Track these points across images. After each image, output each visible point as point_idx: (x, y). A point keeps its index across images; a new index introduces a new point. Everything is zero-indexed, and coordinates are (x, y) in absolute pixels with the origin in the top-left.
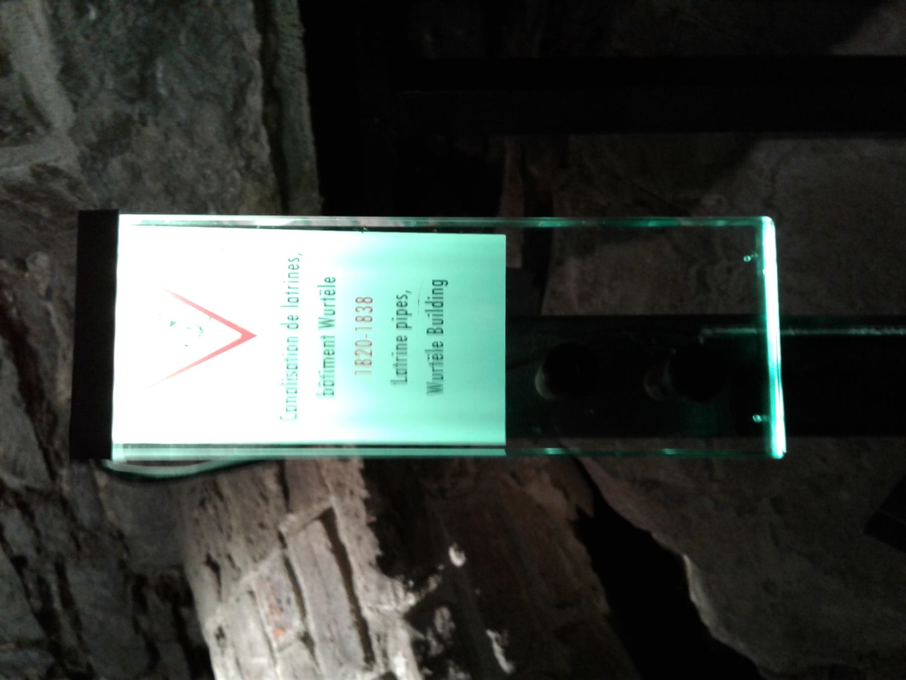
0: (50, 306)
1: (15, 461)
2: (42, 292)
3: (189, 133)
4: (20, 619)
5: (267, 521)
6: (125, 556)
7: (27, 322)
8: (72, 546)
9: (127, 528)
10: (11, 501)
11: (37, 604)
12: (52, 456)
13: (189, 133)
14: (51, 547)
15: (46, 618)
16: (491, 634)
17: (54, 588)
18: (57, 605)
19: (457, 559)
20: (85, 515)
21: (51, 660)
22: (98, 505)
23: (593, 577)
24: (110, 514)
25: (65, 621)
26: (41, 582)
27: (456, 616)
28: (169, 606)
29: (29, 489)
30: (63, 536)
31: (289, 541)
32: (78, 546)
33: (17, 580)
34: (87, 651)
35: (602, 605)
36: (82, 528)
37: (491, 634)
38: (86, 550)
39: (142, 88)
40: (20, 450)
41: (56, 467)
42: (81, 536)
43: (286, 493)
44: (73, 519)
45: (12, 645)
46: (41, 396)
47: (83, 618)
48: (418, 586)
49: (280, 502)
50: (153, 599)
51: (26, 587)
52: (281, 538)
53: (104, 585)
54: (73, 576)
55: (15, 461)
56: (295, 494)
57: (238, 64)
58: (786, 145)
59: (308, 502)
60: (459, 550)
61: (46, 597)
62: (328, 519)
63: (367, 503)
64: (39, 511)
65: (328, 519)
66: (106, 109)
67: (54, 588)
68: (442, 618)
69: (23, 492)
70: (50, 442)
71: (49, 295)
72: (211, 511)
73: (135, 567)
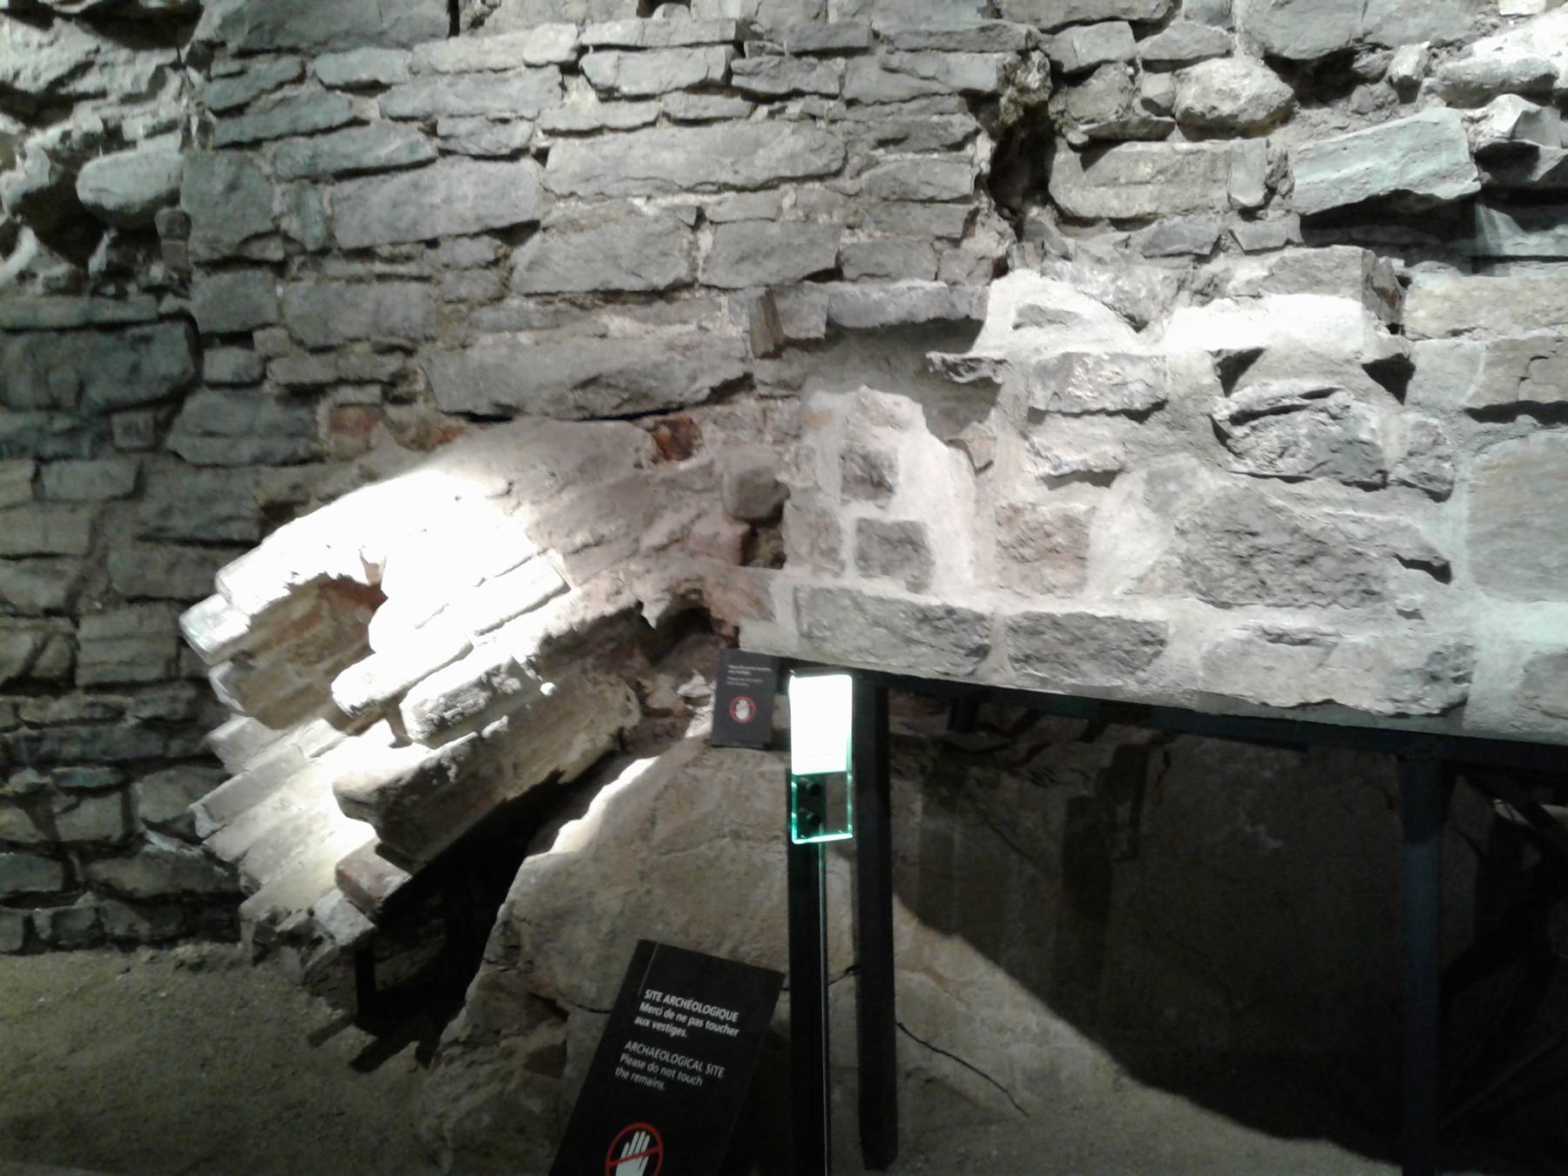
0: (692, 327)
1: (543, 265)
2: (704, 324)
3: (861, 634)
4: (365, 229)
5: (555, 537)
6: (439, 344)
7: (676, 304)
8: (453, 297)
9: (474, 354)
10: (501, 252)
11: (385, 251)
12: (548, 298)
13: (861, 634)
14: (449, 277)
15: (365, 253)
16: (505, 719)
17: (401, 269)
18: (379, 267)
19: (547, 688)
20: (487, 315)
21: (311, 247)
22: (497, 328)
23: (526, 788)
24: (488, 339)
25: (358, 268)
26: (408, 258)
27: (516, 693)
28: (386, 379)
29: (512, 269)
30: (463, 291)
31: (543, 558)
32: (449, 302)
33: (412, 237)
34: (318, 282)
35: (512, 795)
36: (472, 309)
37: (1274, 844)
38: (447, 309)
39: (877, 623)
40: (557, 274)
41: (539, 299)
42: (463, 308)
43: (576, 552)
44: (482, 304)
45: (329, 212)
46: (607, 301)
47: (363, 286)
48: (530, 664)
49: (570, 549)
50: (393, 363)
51: (403, 243)
52: (544, 551)
53: (406, 318)
54: (415, 287)
55: (543, 265)
56: (575, 558)
57: (885, 657)
58: (848, 877)
59: (572, 570)
60: (553, 691)
61: (392, 260)
62: (565, 589)
63: (583, 622)
64: (493, 275)
65: (565, 589)
66: (870, 607)
67: (401, 269)
68: (513, 684)
69: (509, 263)
70: (563, 300)
71: (701, 328)
72: (547, 483)
73: (425, 349)
